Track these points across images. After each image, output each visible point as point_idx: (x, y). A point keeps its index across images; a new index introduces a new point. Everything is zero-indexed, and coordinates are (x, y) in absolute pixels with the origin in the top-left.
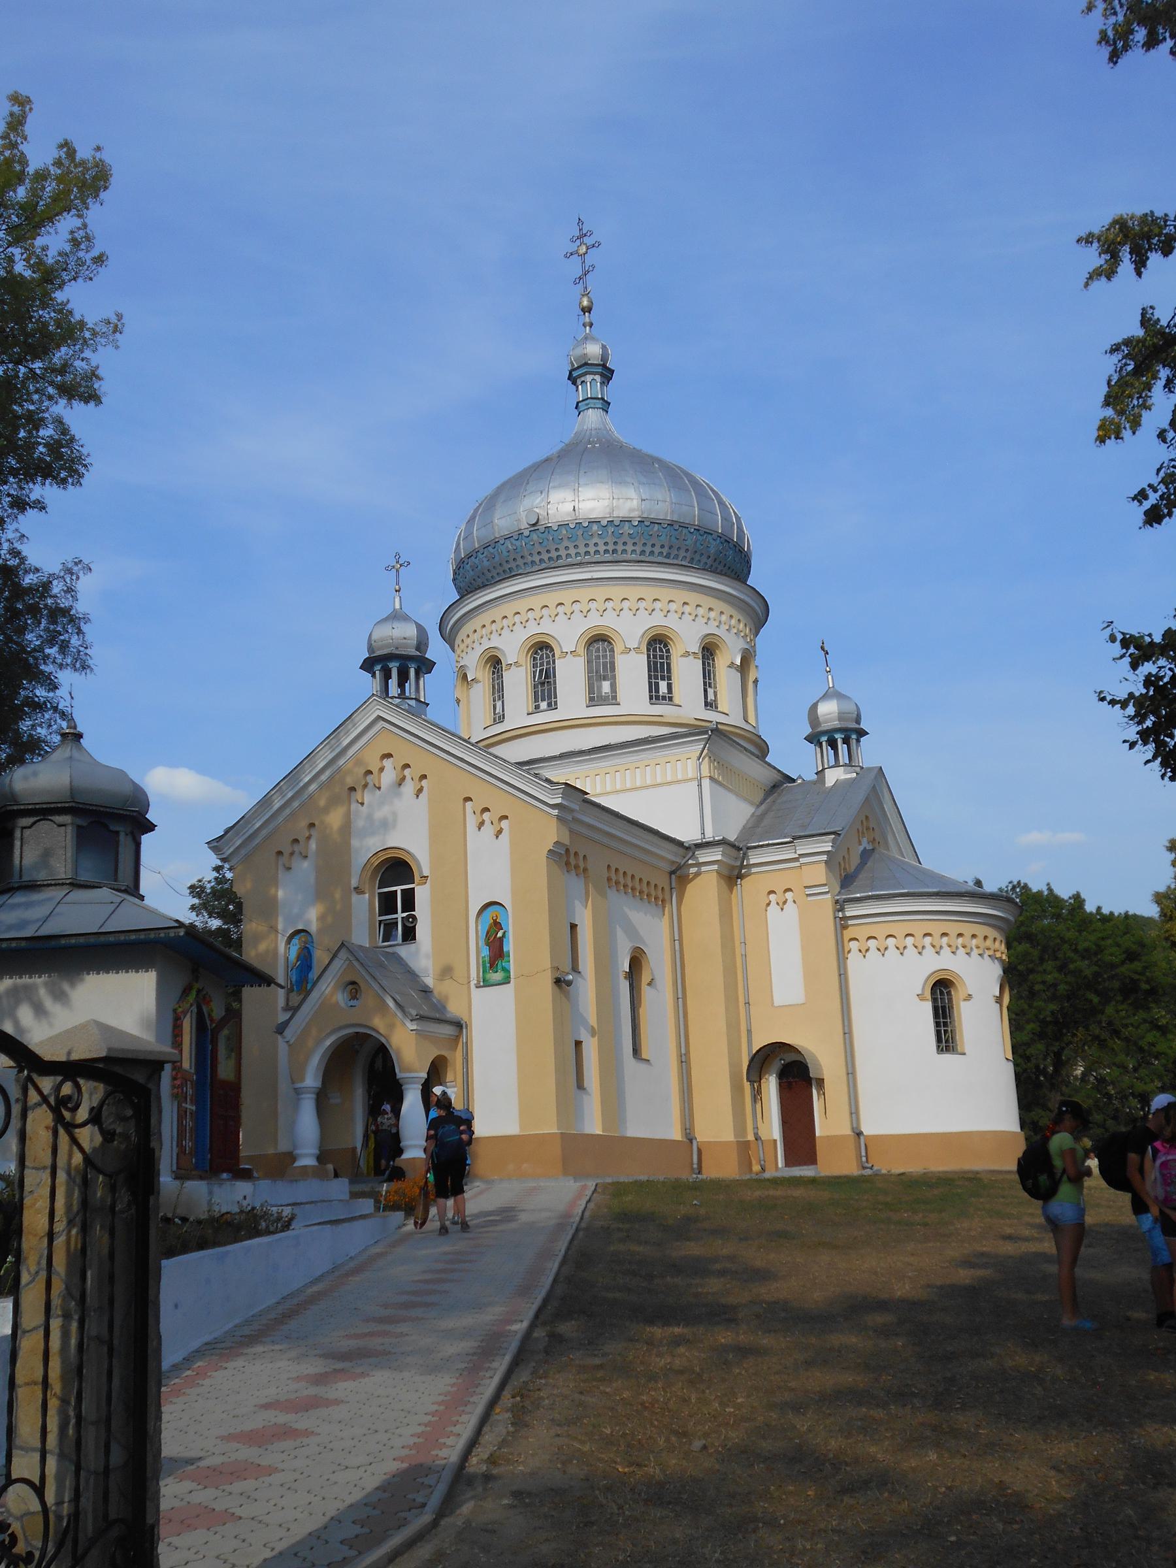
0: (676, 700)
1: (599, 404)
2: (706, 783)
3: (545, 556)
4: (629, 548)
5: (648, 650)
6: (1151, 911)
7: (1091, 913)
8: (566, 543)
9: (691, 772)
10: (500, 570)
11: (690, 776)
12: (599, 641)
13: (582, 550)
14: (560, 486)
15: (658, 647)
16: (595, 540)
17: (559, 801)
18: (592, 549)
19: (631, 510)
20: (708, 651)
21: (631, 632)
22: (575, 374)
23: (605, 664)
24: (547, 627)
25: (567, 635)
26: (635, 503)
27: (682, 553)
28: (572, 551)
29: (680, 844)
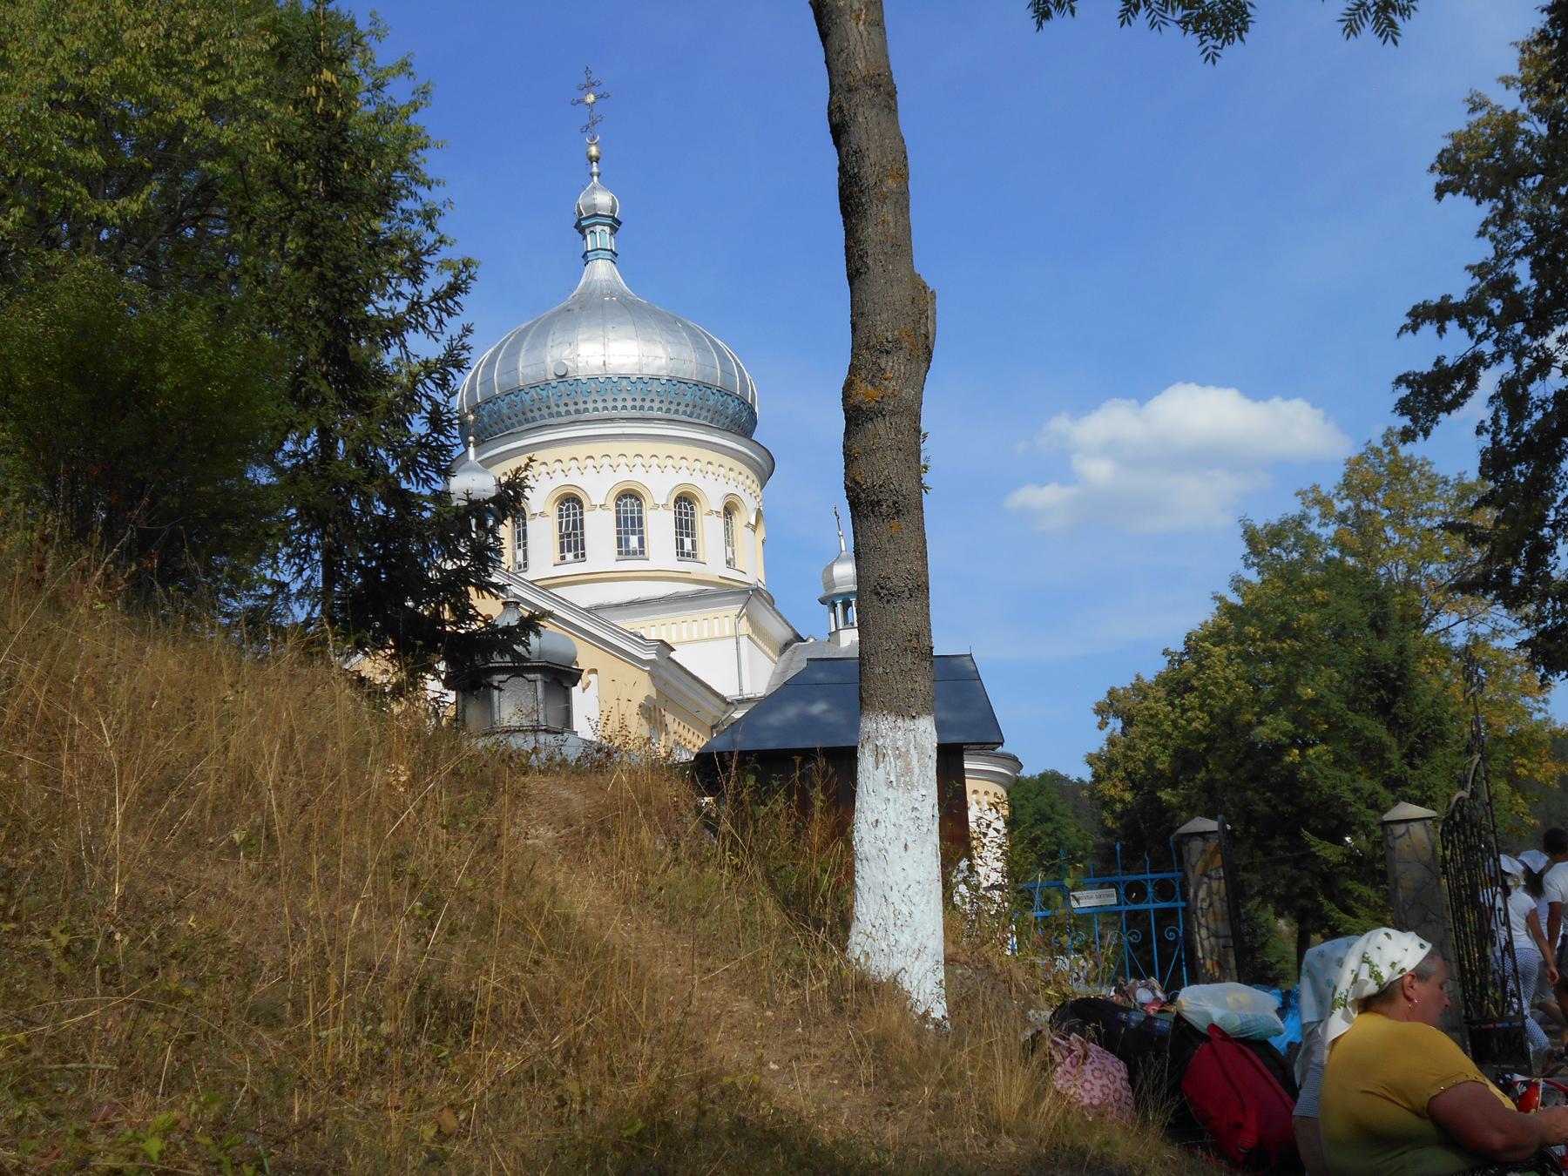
0: (700, 558)
1: (608, 255)
2: (744, 641)
3: (572, 408)
4: (656, 405)
5: (617, 505)
6: (1086, 774)
7: (1104, 764)
8: (594, 396)
9: (728, 630)
10: (521, 417)
11: (727, 633)
12: (630, 496)
13: (610, 404)
14: (588, 340)
15: (685, 501)
16: (624, 395)
17: (653, 657)
18: (620, 404)
19: (660, 368)
20: (729, 510)
21: (659, 488)
22: (584, 223)
23: (633, 519)
24: (575, 479)
25: (598, 489)
26: (693, 367)
27: (704, 413)
28: (600, 405)
29: (723, 699)
